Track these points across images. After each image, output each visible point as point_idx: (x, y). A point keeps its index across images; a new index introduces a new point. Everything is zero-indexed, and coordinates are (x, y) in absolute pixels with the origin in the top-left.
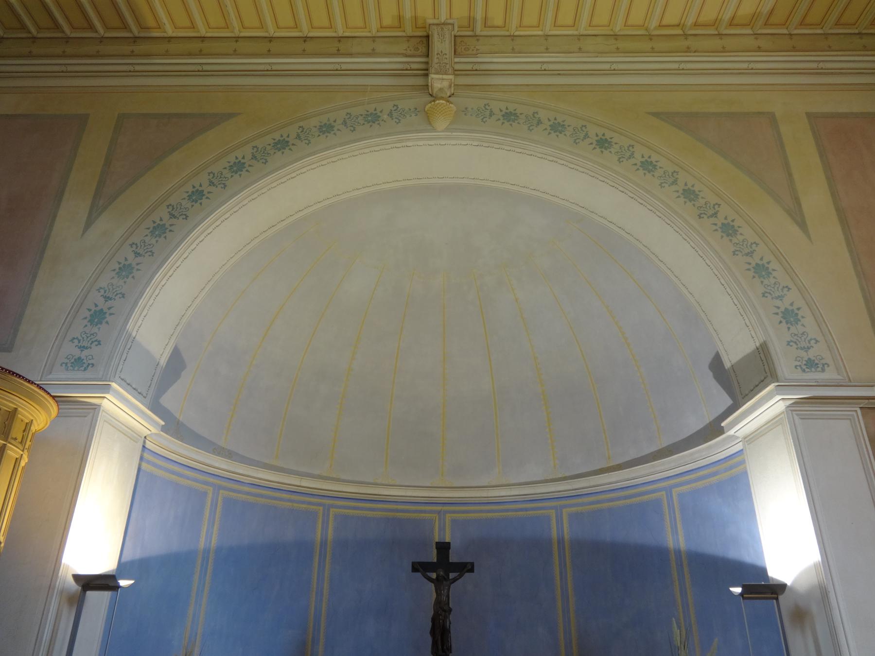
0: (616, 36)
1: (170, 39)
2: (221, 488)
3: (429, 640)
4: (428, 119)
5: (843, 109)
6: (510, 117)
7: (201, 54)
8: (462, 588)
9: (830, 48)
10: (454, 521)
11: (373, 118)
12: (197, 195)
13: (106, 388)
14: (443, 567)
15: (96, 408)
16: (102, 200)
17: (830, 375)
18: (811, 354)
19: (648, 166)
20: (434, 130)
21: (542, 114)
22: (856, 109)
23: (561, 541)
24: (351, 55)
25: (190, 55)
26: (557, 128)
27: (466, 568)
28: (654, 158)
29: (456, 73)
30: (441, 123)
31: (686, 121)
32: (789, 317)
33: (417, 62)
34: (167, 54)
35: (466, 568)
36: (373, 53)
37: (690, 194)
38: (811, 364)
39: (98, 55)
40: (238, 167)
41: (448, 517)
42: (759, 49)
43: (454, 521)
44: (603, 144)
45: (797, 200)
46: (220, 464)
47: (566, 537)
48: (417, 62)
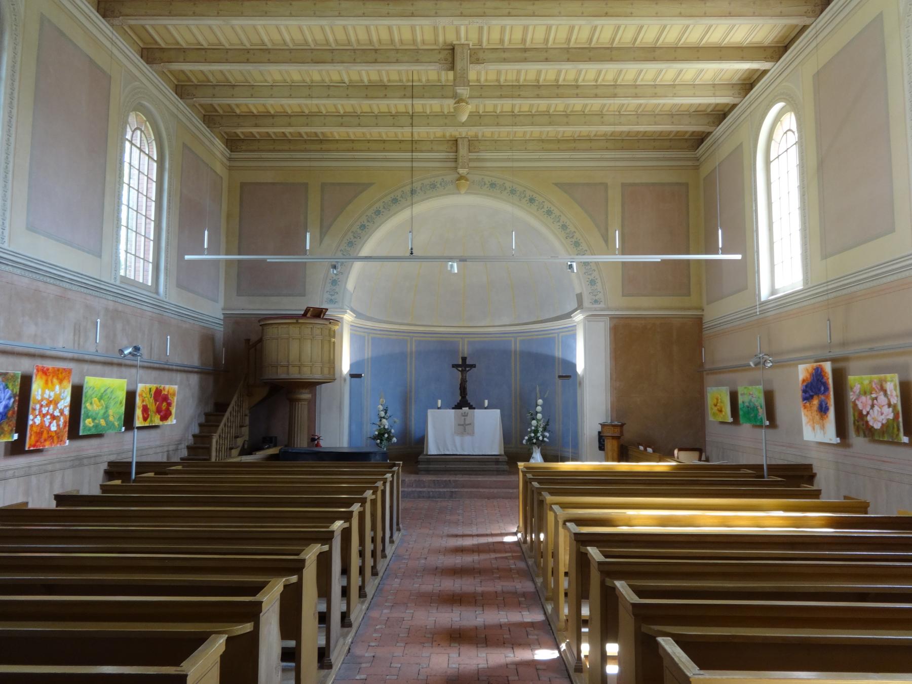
0: (543, 141)
1: (337, 141)
2: (369, 333)
3: (459, 391)
4: (458, 188)
5: (637, 181)
6: (493, 185)
7: (353, 150)
8: (471, 374)
9: (639, 148)
10: (469, 342)
11: (433, 186)
12: (363, 227)
13: (346, 312)
14: (464, 366)
15: (342, 318)
16: (324, 230)
17: (602, 305)
18: (597, 298)
19: (549, 213)
20: (460, 193)
21: (508, 184)
22: (644, 181)
23: (515, 351)
24: (421, 151)
25: (349, 151)
26: (513, 192)
27: (473, 366)
28: (553, 208)
29: (469, 168)
30: (463, 191)
31: (567, 188)
32: (592, 282)
33: (452, 155)
34: (337, 150)
35: (473, 366)
36: (431, 151)
37: (564, 227)
38: (596, 301)
39: (305, 150)
40: (378, 213)
41: (466, 340)
42: (607, 149)
43: (469, 342)
44: (532, 200)
45: (607, 230)
46: (369, 324)
47: (518, 349)
48: (452, 155)
